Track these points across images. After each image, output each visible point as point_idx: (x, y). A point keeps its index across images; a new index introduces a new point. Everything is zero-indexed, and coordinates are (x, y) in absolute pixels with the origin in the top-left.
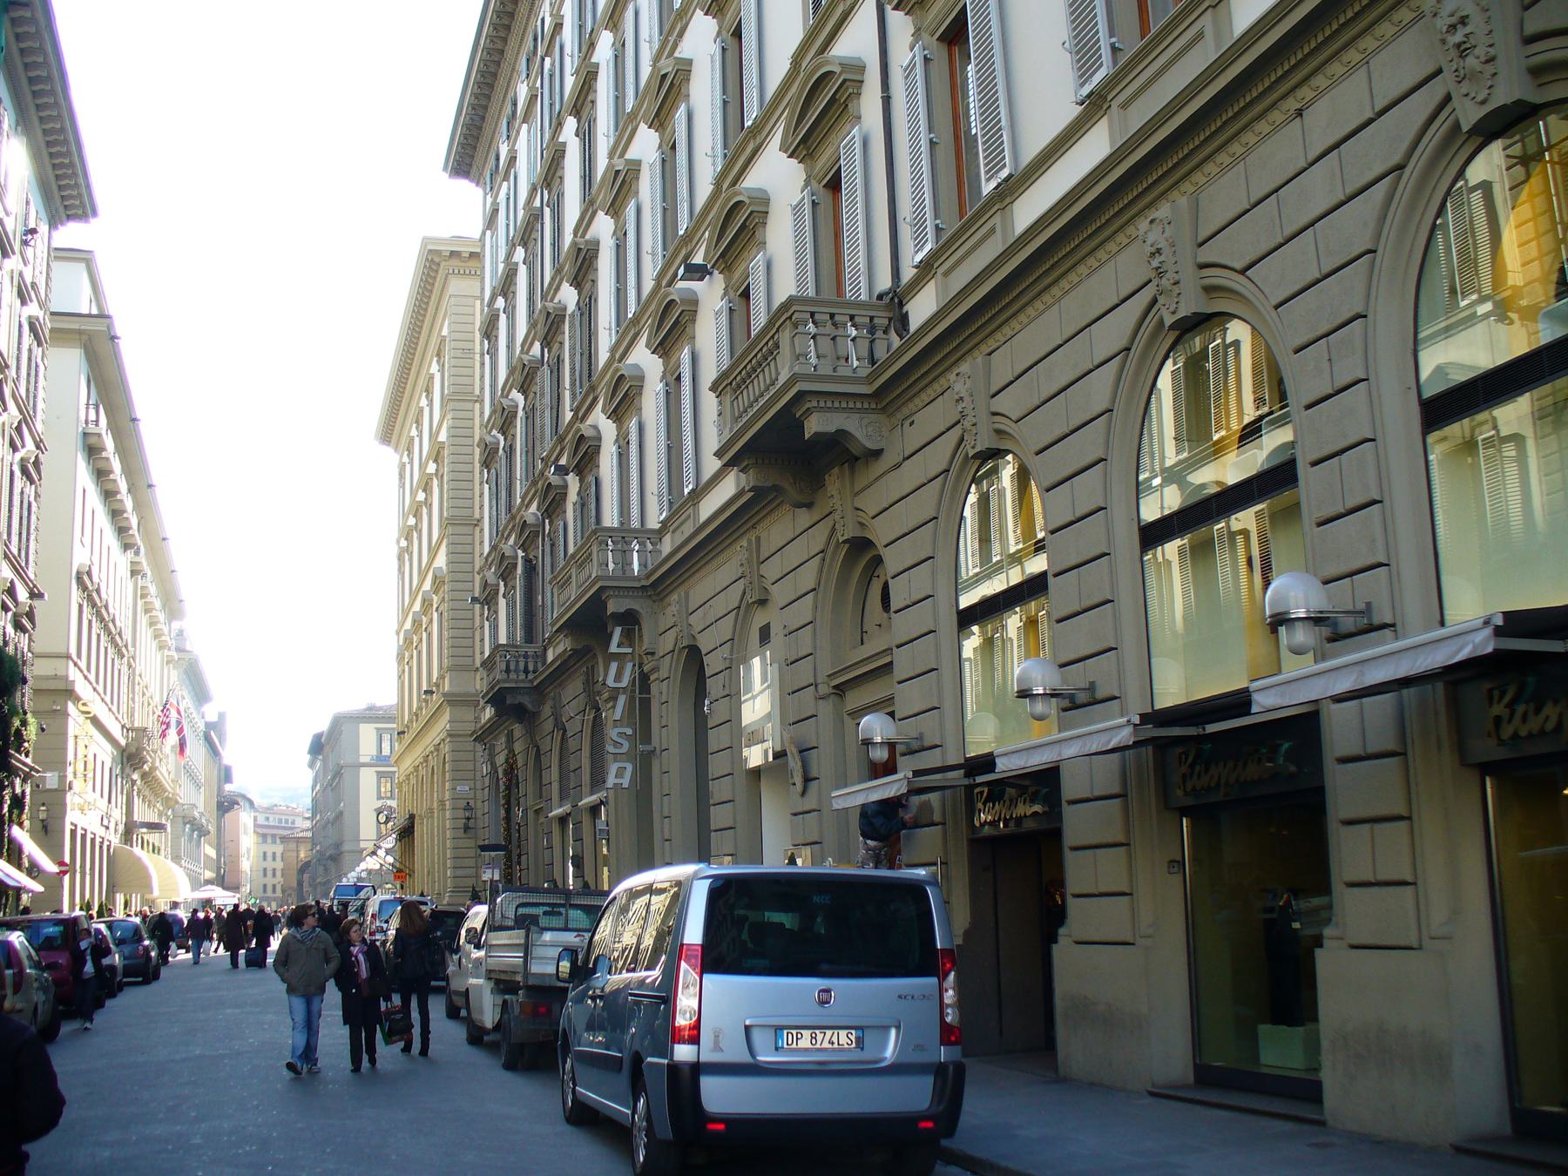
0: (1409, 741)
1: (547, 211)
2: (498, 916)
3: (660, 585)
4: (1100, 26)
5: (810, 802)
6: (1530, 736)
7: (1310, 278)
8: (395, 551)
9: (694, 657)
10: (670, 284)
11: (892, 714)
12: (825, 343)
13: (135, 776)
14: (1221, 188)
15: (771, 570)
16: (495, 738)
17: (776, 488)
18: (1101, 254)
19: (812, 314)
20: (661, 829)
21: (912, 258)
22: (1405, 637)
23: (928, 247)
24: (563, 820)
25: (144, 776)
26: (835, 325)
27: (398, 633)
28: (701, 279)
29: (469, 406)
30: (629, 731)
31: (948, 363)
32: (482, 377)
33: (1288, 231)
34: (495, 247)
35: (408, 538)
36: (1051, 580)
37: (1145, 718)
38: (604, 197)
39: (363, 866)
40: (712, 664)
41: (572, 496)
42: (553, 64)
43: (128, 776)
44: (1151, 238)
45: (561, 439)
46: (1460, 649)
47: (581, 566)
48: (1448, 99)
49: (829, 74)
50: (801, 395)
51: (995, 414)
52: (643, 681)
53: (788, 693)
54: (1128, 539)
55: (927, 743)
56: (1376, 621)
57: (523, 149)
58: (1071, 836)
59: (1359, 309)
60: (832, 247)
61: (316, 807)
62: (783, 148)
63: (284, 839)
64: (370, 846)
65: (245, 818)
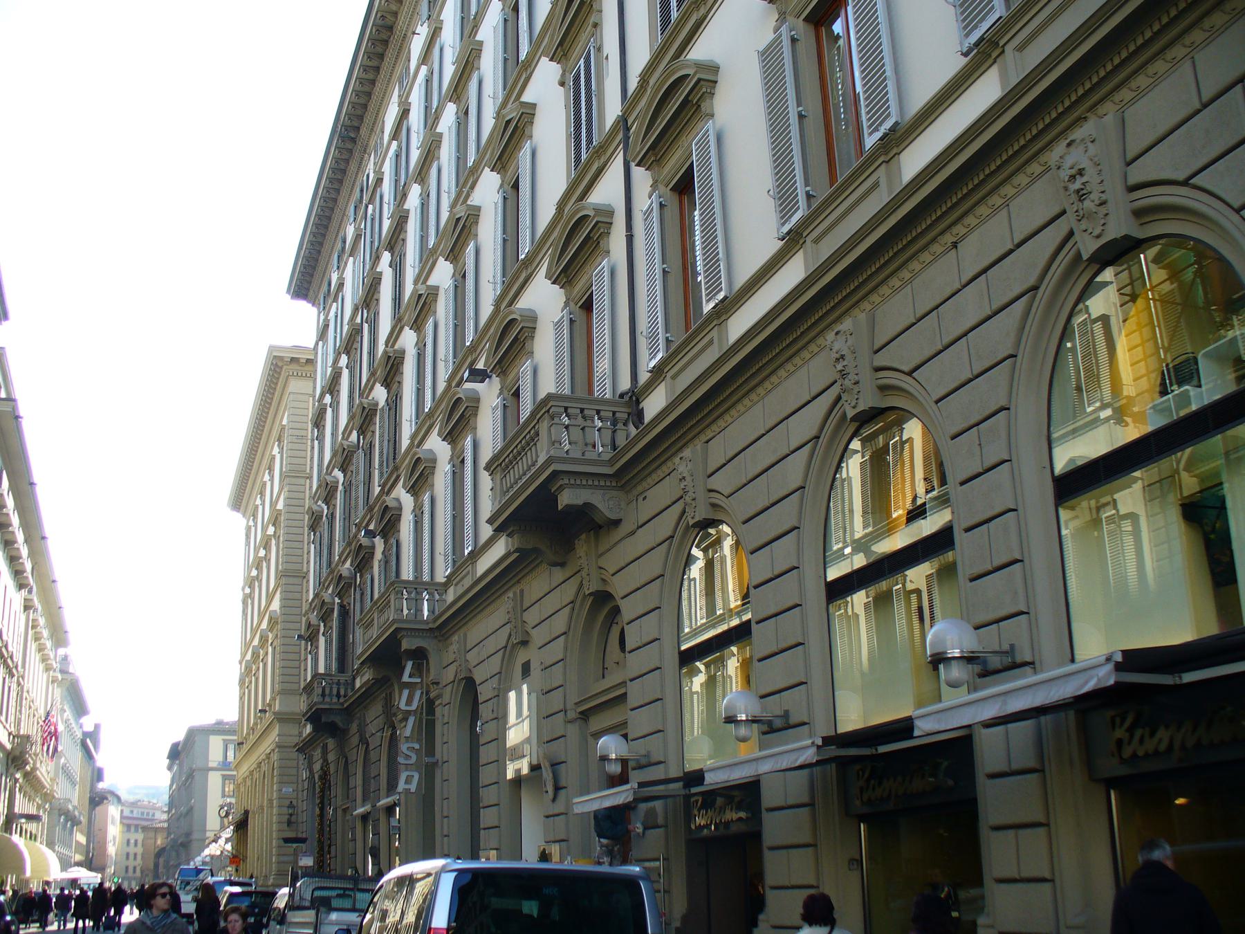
0: (1046, 758)
1: (366, 326)
2: (297, 898)
3: (445, 627)
4: (797, 177)
5: (559, 807)
6: (1147, 755)
7: (963, 378)
8: (240, 596)
9: (470, 685)
10: (458, 385)
11: (625, 736)
12: (576, 432)
13: (18, 776)
14: (895, 305)
15: (532, 617)
16: (314, 749)
17: (536, 551)
18: (797, 360)
19: (566, 409)
20: (441, 826)
21: (648, 363)
22: (1042, 671)
23: (660, 356)
24: (365, 818)
25: (26, 775)
26: (584, 417)
27: (241, 663)
28: (482, 381)
29: (302, 481)
30: (417, 746)
31: (674, 450)
32: (312, 458)
33: (946, 341)
34: (325, 354)
35: (251, 586)
36: (754, 626)
37: (827, 741)
38: (410, 316)
39: (207, 852)
40: (484, 692)
41: (378, 555)
42: (374, 211)
43: (13, 775)
44: (836, 347)
45: (371, 509)
46: (1086, 682)
47: (381, 611)
48: (1071, 234)
49: (585, 217)
50: (555, 474)
51: (710, 491)
52: (430, 706)
53: (543, 717)
54: (816, 595)
55: (653, 760)
56: (1019, 660)
57: (351, 276)
58: (769, 838)
59: (1003, 403)
60: (585, 356)
61: (172, 803)
62: (548, 276)
63: (145, 829)
64: (210, 835)
65: (113, 811)
